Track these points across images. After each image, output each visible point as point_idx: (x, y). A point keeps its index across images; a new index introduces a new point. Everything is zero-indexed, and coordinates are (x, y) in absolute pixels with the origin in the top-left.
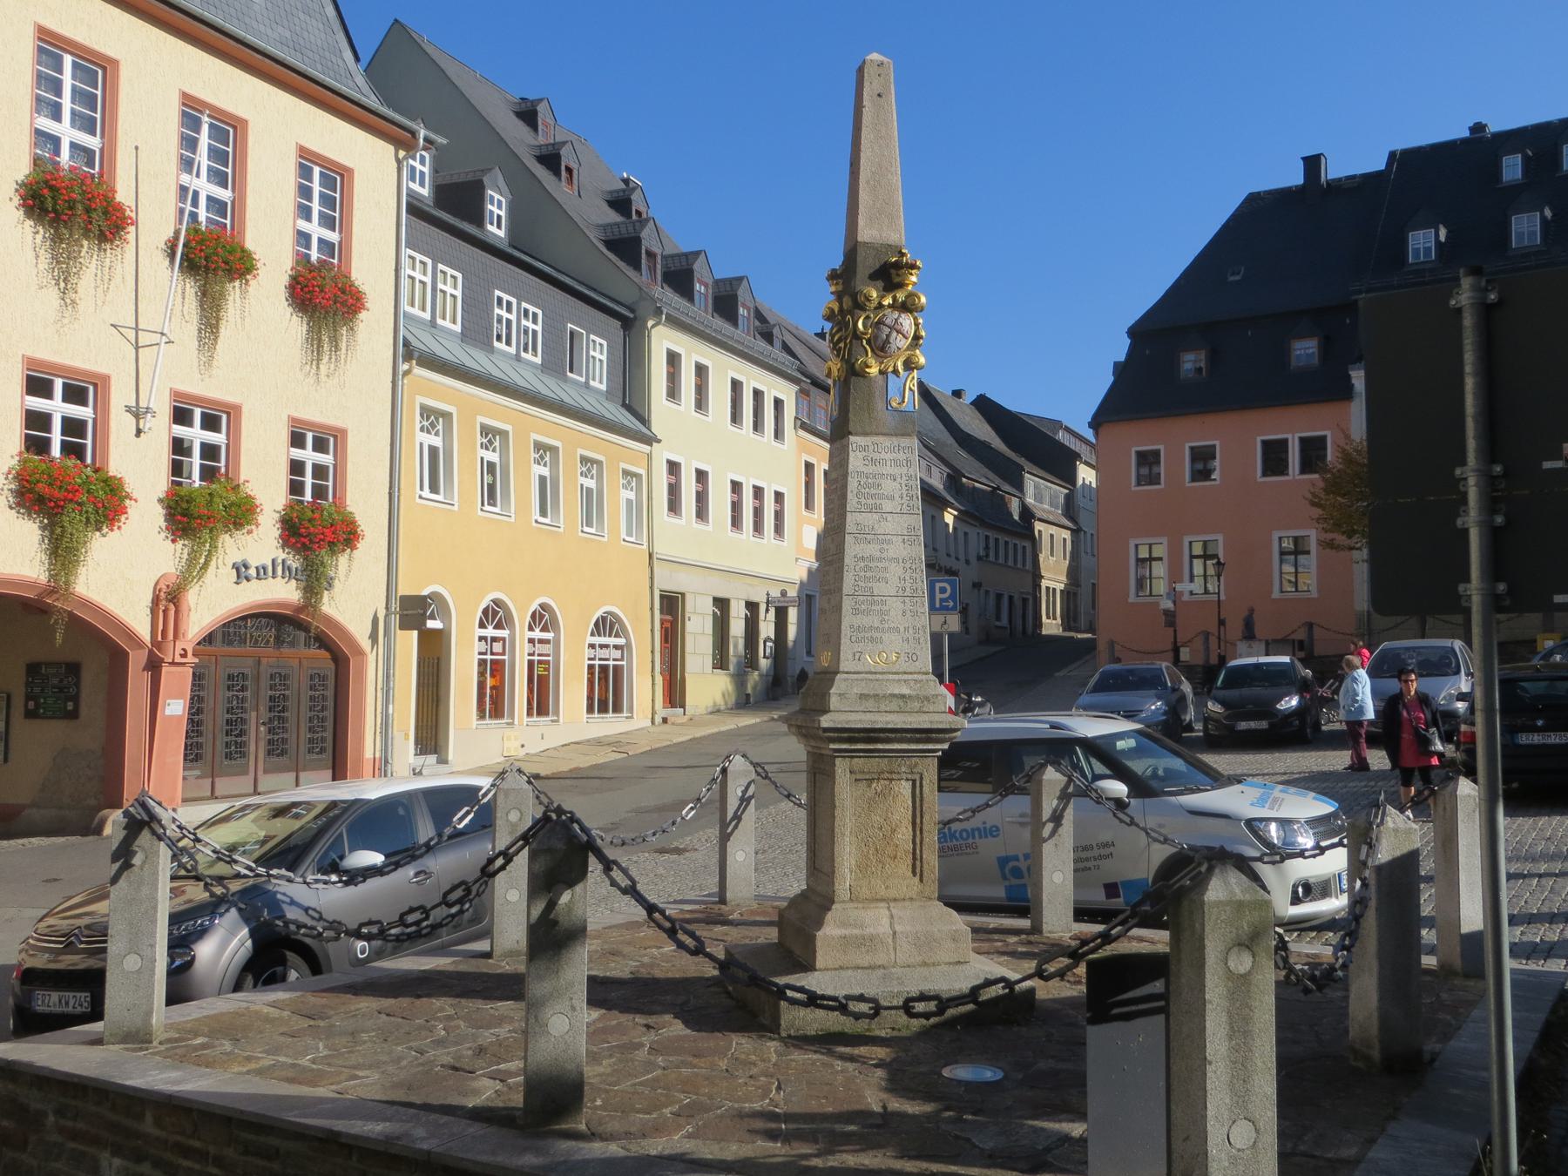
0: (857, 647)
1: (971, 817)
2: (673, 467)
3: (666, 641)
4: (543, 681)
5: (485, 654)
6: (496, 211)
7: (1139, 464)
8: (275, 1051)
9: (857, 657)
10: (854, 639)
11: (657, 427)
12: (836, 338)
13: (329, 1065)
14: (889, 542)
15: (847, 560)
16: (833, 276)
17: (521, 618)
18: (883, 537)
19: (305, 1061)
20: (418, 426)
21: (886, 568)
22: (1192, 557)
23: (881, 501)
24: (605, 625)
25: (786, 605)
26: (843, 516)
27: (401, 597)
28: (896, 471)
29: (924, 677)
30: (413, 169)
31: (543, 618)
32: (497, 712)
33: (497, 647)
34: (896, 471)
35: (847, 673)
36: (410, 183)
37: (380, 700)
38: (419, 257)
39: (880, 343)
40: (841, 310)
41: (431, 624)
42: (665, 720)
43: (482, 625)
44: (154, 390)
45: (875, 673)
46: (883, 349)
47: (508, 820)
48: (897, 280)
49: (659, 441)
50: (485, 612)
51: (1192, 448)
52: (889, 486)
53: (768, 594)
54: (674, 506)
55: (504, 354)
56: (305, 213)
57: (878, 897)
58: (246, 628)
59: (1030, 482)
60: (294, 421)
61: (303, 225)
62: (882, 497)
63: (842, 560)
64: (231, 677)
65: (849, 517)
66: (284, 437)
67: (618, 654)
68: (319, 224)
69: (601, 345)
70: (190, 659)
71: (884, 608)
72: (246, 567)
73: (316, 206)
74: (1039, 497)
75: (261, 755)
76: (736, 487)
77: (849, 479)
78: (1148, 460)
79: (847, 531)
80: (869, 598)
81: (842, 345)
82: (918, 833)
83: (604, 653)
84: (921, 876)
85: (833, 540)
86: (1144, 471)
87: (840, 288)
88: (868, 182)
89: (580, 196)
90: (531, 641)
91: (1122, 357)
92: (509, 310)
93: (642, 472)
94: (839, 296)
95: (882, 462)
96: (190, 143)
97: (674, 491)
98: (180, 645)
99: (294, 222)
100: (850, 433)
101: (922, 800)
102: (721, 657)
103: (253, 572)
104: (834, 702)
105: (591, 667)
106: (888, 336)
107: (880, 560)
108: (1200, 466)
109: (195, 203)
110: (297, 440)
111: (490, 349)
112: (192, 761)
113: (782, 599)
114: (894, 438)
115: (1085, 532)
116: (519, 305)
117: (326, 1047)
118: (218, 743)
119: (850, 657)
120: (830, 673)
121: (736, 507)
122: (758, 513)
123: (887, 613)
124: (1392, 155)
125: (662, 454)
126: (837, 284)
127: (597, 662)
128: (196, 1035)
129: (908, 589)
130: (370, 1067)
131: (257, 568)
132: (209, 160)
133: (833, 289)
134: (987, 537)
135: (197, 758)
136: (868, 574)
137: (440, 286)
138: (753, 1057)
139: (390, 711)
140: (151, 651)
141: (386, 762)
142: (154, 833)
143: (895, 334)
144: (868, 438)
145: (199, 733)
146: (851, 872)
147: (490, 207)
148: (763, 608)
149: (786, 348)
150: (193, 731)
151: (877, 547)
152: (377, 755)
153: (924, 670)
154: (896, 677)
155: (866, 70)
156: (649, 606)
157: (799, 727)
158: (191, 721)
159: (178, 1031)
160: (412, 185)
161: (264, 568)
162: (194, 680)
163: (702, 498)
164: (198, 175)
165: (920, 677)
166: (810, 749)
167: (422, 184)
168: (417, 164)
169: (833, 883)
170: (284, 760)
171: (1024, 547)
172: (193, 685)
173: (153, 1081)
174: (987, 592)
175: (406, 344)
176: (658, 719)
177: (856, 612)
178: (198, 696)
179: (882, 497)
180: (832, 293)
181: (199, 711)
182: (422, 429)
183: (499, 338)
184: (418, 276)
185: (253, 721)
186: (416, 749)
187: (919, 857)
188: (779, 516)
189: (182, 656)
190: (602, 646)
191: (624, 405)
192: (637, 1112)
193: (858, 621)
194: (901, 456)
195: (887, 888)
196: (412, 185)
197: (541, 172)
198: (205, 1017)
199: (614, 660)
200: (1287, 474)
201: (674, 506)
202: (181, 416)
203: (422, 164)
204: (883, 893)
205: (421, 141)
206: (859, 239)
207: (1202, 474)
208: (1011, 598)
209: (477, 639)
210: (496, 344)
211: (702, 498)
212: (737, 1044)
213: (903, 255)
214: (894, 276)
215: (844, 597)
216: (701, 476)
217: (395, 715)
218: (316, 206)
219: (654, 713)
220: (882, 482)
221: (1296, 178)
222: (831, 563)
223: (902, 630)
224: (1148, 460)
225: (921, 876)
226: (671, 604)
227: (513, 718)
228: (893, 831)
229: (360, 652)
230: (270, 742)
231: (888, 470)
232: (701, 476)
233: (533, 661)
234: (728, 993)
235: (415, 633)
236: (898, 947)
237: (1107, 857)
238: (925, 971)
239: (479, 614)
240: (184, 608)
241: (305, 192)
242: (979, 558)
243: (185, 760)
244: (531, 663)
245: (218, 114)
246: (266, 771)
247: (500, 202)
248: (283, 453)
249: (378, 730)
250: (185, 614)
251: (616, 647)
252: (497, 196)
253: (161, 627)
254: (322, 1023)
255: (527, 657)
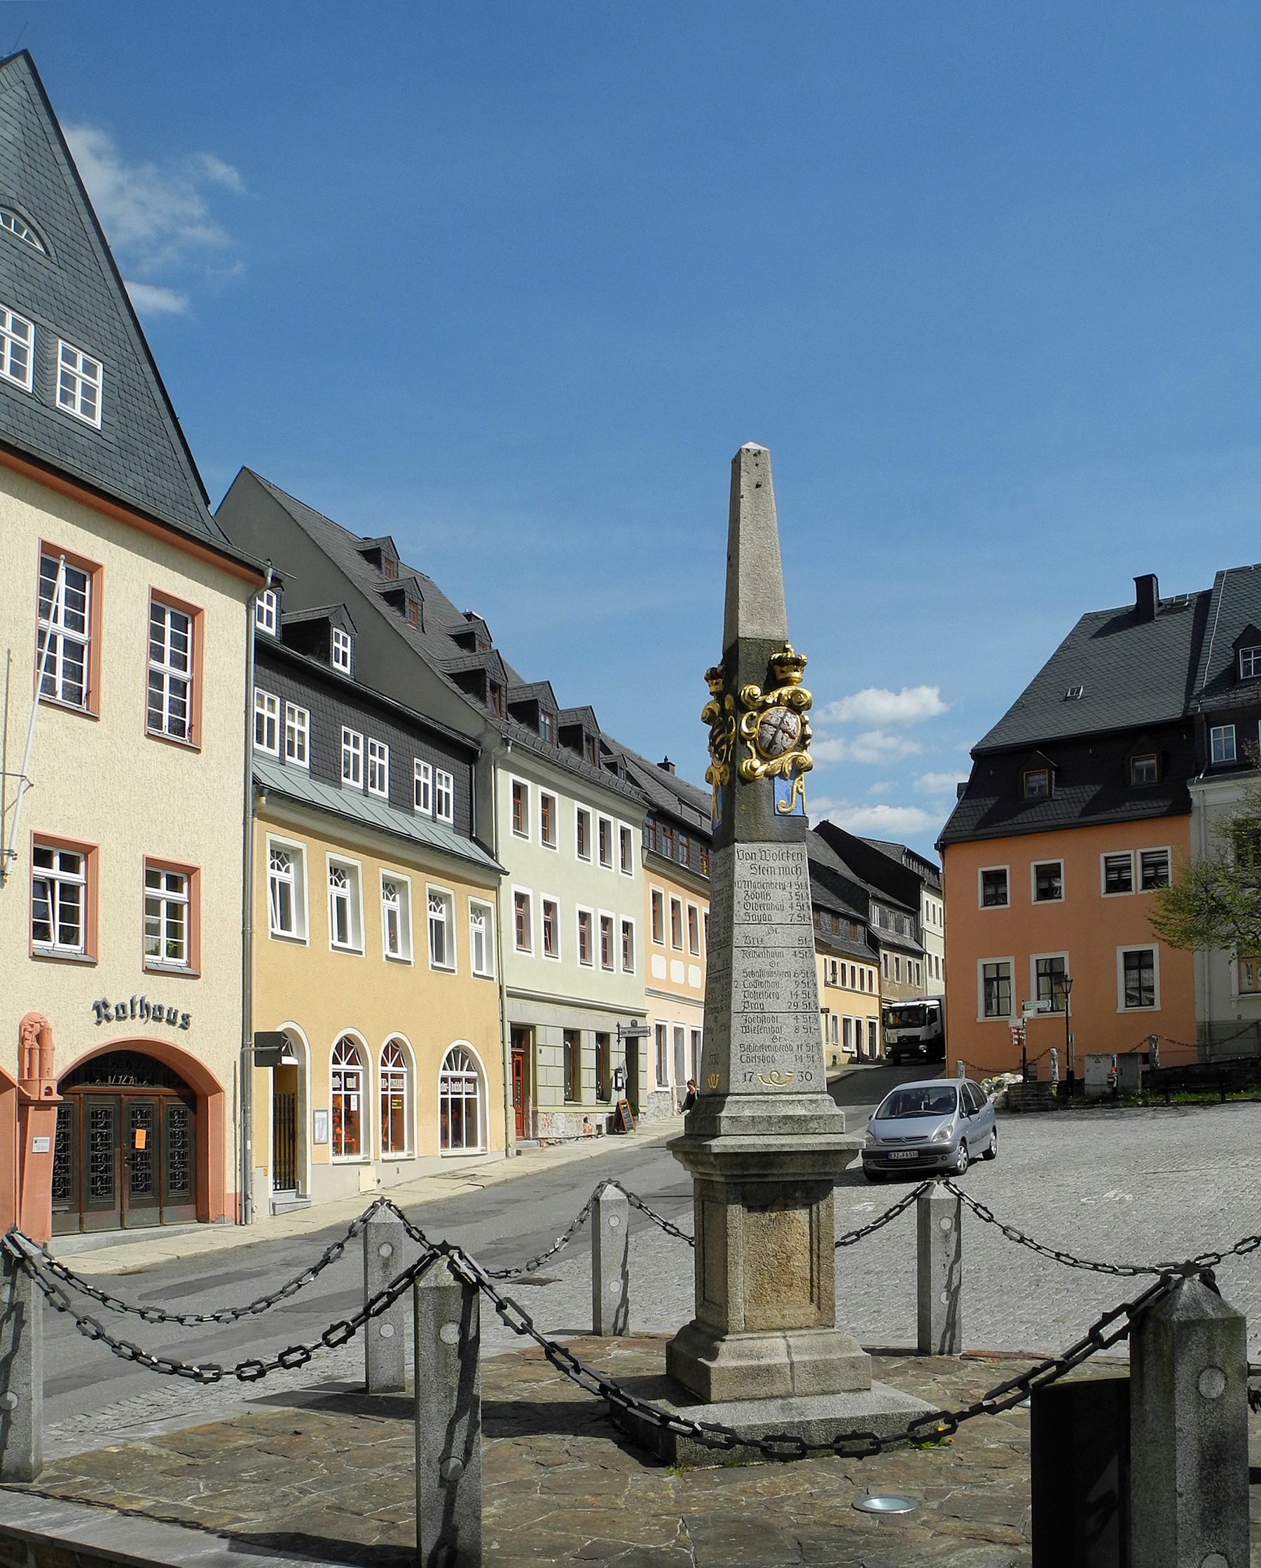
0: (749, 1067)
1: (855, 1240)
2: (521, 899)
3: (518, 1074)
4: (397, 1115)
5: (340, 1089)
6: (342, 648)
7: (985, 885)
8: (157, 1489)
9: (748, 1078)
10: (744, 1059)
11: (504, 861)
12: (718, 740)
13: (211, 1506)
14: (780, 955)
15: (735, 976)
16: (712, 675)
17: (374, 1052)
18: (773, 950)
19: (187, 1502)
20: (269, 863)
21: (777, 983)
22: (1039, 975)
23: (770, 912)
24: (458, 1057)
25: (636, 1035)
26: (729, 927)
27: (256, 1033)
28: (785, 879)
29: (819, 1097)
30: (261, 608)
31: (395, 1052)
32: (352, 1148)
33: (351, 1083)
34: (785, 879)
35: (738, 1094)
36: (257, 622)
37: (238, 1136)
38: (267, 695)
39: (765, 744)
40: (723, 712)
41: (286, 1060)
42: (519, 1153)
43: (335, 1061)
44: (15, 832)
45: (768, 1094)
46: (768, 750)
47: (379, 1255)
48: (781, 677)
49: (507, 874)
50: (338, 1047)
51: (1037, 867)
52: (778, 896)
53: (618, 1026)
54: (522, 939)
55: (352, 789)
56: (157, 654)
57: (774, 1326)
58: (107, 1067)
59: (875, 911)
60: (149, 861)
61: (155, 664)
62: (770, 907)
63: (729, 975)
64: (95, 1115)
65: (736, 930)
66: (140, 875)
67: (470, 1088)
68: (171, 665)
69: (447, 779)
70: (56, 1097)
71: (775, 1025)
72: (106, 1005)
73: (167, 647)
74: (884, 923)
75: (126, 1192)
76: (584, 917)
77: (736, 888)
78: (995, 880)
79: (735, 944)
80: (760, 1015)
81: (724, 747)
82: (815, 1259)
83: (456, 1087)
84: (819, 1303)
85: (719, 954)
86: (991, 891)
87: (720, 688)
88: (745, 584)
89: (424, 631)
90: (384, 1076)
91: (966, 779)
92: (356, 745)
93: (492, 905)
94: (720, 697)
95: (770, 870)
96: (47, 589)
97: (522, 922)
98: (45, 1085)
99: (147, 662)
100: (736, 841)
101: (818, 1226)
102: (573, 1089)
103: (112, 1011)
104: (725, 1126)
105: (444, 1102)
106: (774, 736)
107: (770, 974)
108: (1045, 885)
109: (53, 647)
110: (152, 879)
111: (338, 784)
112: (60, 1196)
113: (632, 1030)
114: (782, 845)
115: (930, 955)
116: (366, 740)
117: (206, 1487)
118: (84, 1181)
119: (741, 1077)
120: (719, 1095)
121: (584, 938)
122: (606, 943)
123: (779, 1030)
124: (1219, 575)
125: (510, 887)
126: (716, 683)
127: (450, 1096)
128: (76, 1474)
129: (800, 1004)
130: (254, 1509)
131: (117, 1008)
132: (66, 605)
133: (713, 689)
134: (834, 963)
135: (64, 1195)
136: (758, 990)
137: (288, 723)
138: (652, 1495)
139: (249, 1148)
140: (20, 1092)
141: (247, 1197)
142: (26, 1271)
143: (780, 733)
144: (755, 845)
145: (67, 1170)
146: (745, 1301)
147: (335, 644)
148: (614, 1038)
149: (630, 777)
150: (60, 1168)
151: (768, 961)
152: (238, 1191)
153: (818, 1089)
154: (790, 1098)
155: (742, 460)
156: (500, 1039)
157: (686, 1154)
158: (57, 1158)
159: (57, 1468)
160: (259, 625)
161: (123, 1007)
162: (59, 1117)
163: (549, 927)
164: (55, 621)
165: (814, 1097)
166: (698, 1176)
167: (269, 624)
168: (264, 605)
169: (727, 1314)
170: (148, 1196)
171: (870, 972)
172: (59, 1123)
173: (35, 1522)
174: (835, 1018)
175: (256, 781)
176: (512, 1151)
177: (746, 1030)
178: (64, 1133)
179: (770, 907)
180: (711, 694)
181: (65, 1148)
182: (272, 866)
183: (347, 776)
184: (266, 713)
185: (117, 1157)
186: (275, 1184)
187: (816, 1285)
188: (627, 946)
189: (46, 1094)
190: (454, 1080)
191: (472, 839)
192: (539, 1556)
193: (748, 1039)
194: (791, 863)
195: (783, 1317)
196: (259, 625)
197: (383, 607)
198: (84, 1454)
199: (467, 1093)
200: (1131, 890)
201: (522, 939)
202: (41, 858)
203: (268, 604)
204: (779, 1322)
205: (269, 579)
206: (740, 635)
207: (1046, 893)
208: (858, 1023)
209: (331, 1075)
210: (344, 779)
211: (549, 927)
212: (633, 1480)
213: (786, 650)
214: (778, 672)
215: (733, 1015)
216: (549, 907)
217: (254, 1151)
218: (167, 647)
219: (507, 1146)
220: (771, 891)
221: (1129, 599)
222: (717, 979)
223: (795, 1047)
224: (995, 880)
225: (819, 1303)
226: (521, 1035)
227: (413, 1150)
228: (789, 1258)
229: (217, 1089)
230: (135, 1178)
231: (777, 878)
232: (549, 907)
233: (387, 1095)
234: (615, 1426)
235: (272, 1068)
236: (796, 1377)
237: (811, 1299)
238: (825, 1400)
239: (333, 1049)
240: (47, 1047)
241: (157, 633)
242: (827, 984)
243: (53, 1196)
244: (384, 1097)
245: (72, 558)
246: (131, 1207)
247: (345, 640)
248: (137, 891)
249: (238, 1167)
250: (49, 1052)
251: (468, 1080)
252: (342, 634)
253: (26, 1065)
254: (200, 1462)
255: (381, 1093)
